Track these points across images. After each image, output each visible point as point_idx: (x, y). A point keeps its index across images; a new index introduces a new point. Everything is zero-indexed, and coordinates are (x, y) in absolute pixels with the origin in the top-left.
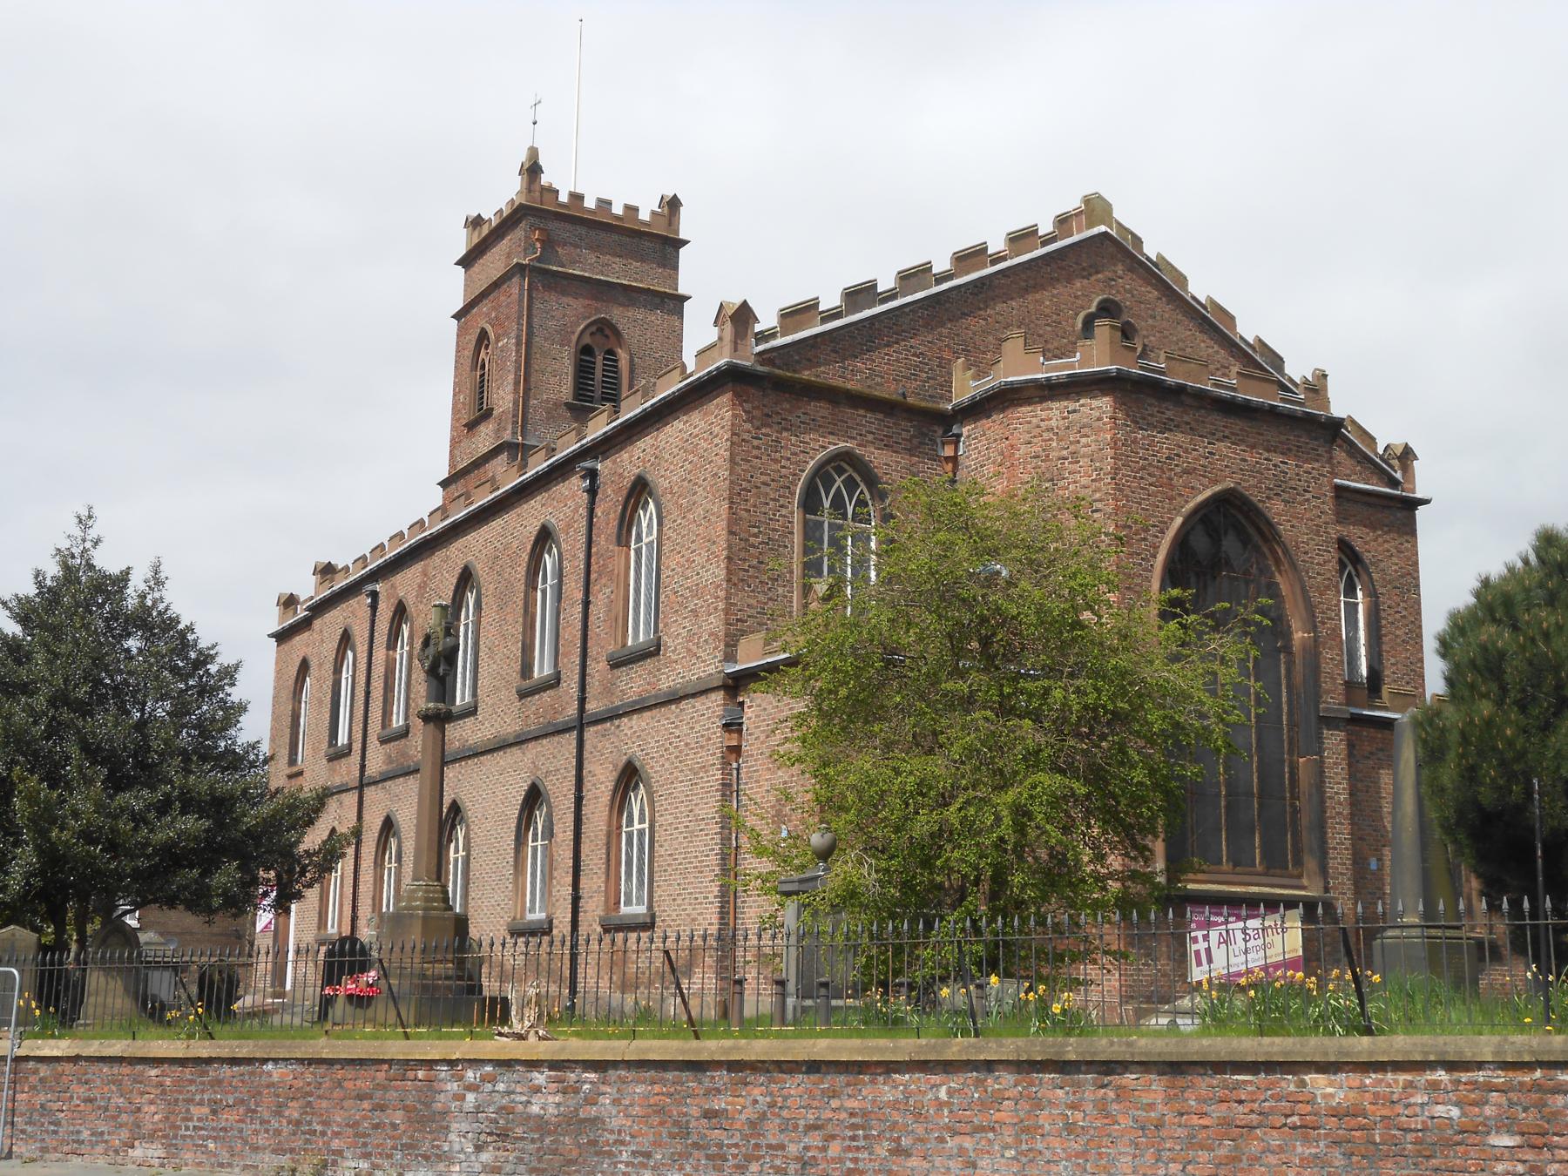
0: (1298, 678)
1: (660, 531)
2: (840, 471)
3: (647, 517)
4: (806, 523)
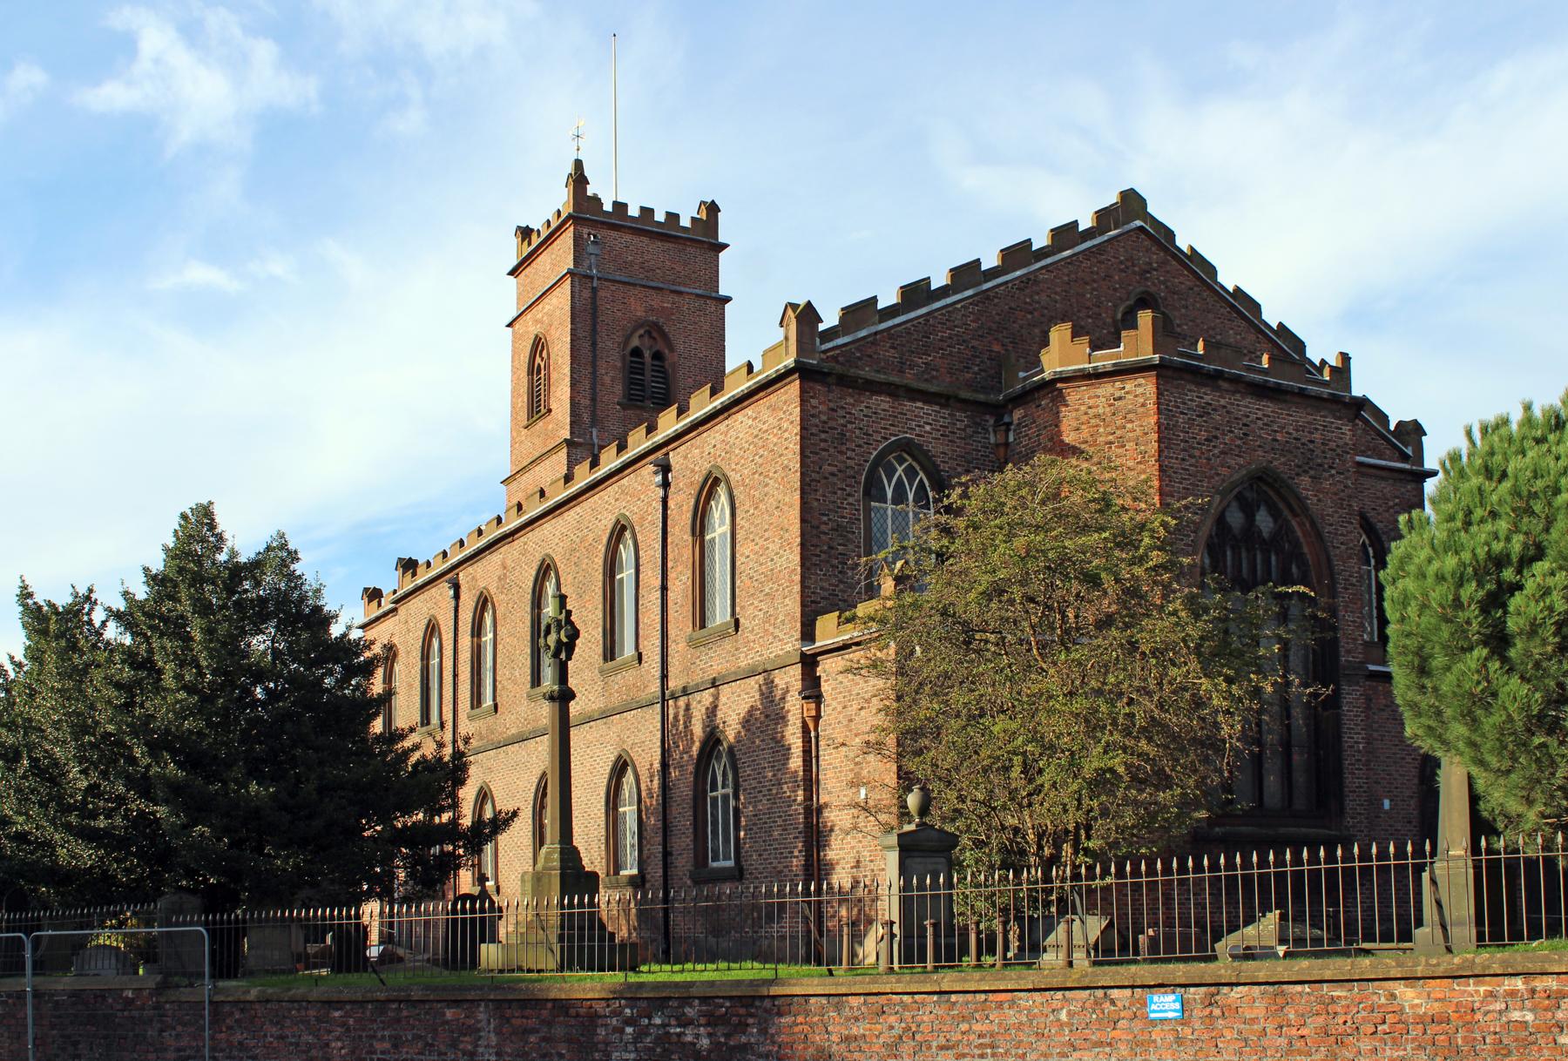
2: (901, 461)
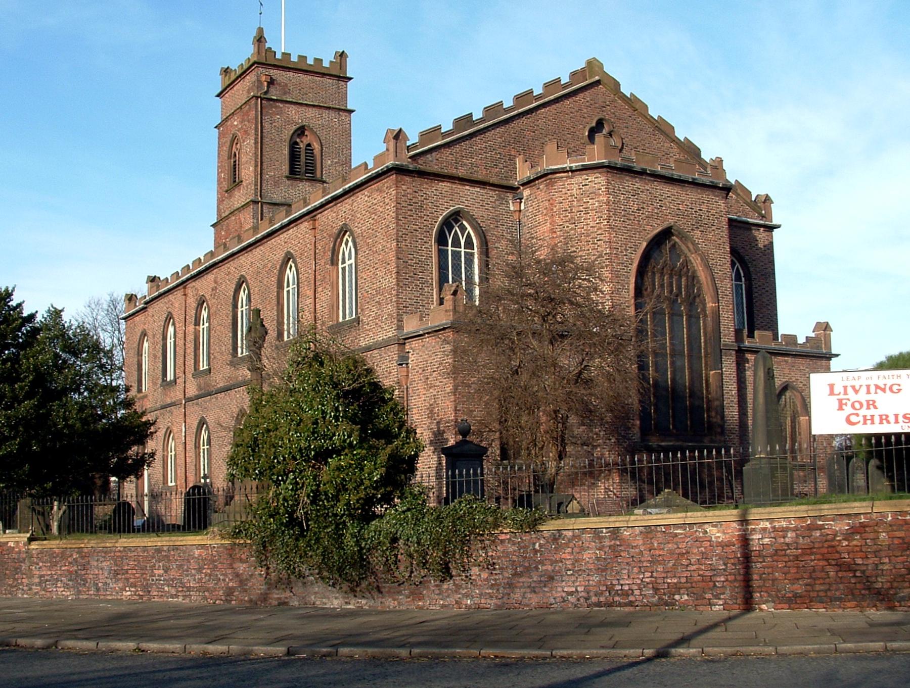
0: (709, 329)
1: (356, 258)
3: (347, 249)
4: (439, 250)
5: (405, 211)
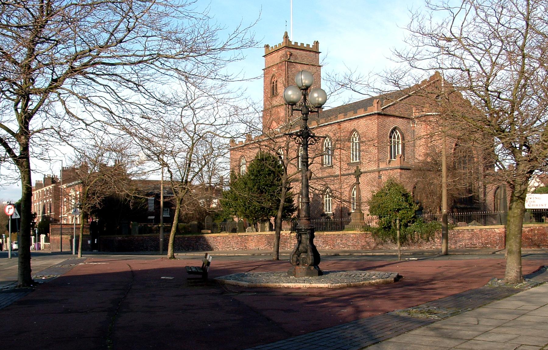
5: (380, 127)
